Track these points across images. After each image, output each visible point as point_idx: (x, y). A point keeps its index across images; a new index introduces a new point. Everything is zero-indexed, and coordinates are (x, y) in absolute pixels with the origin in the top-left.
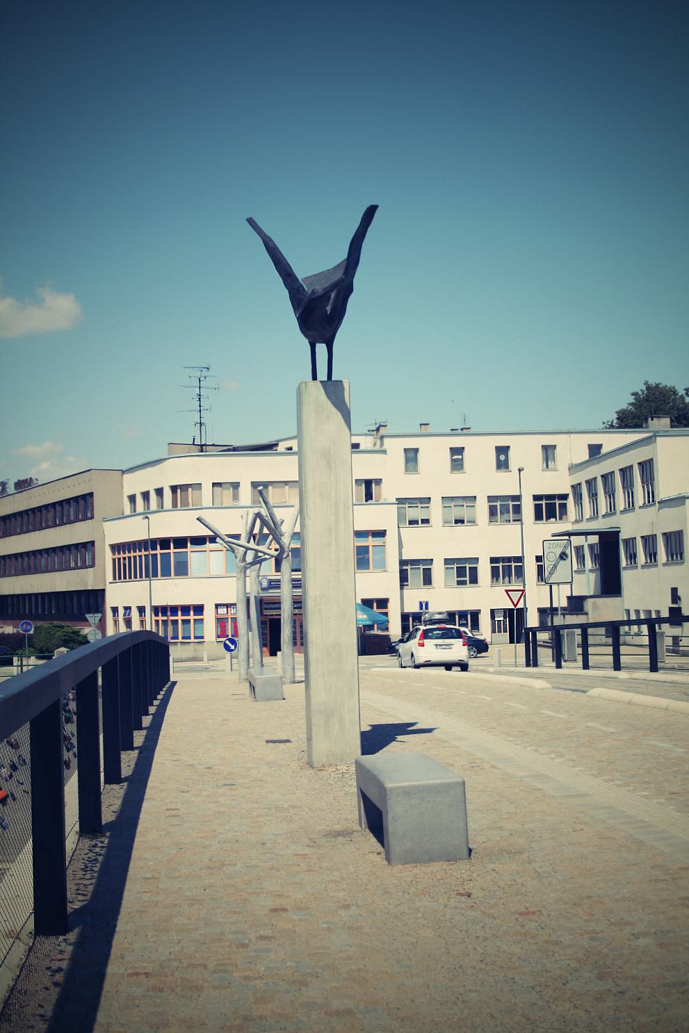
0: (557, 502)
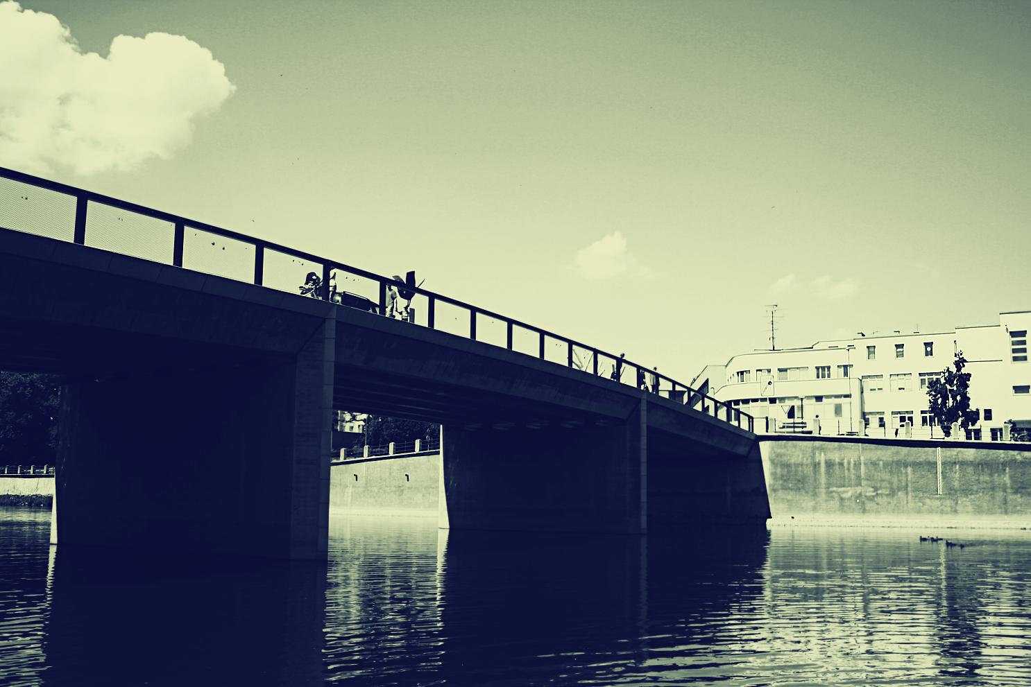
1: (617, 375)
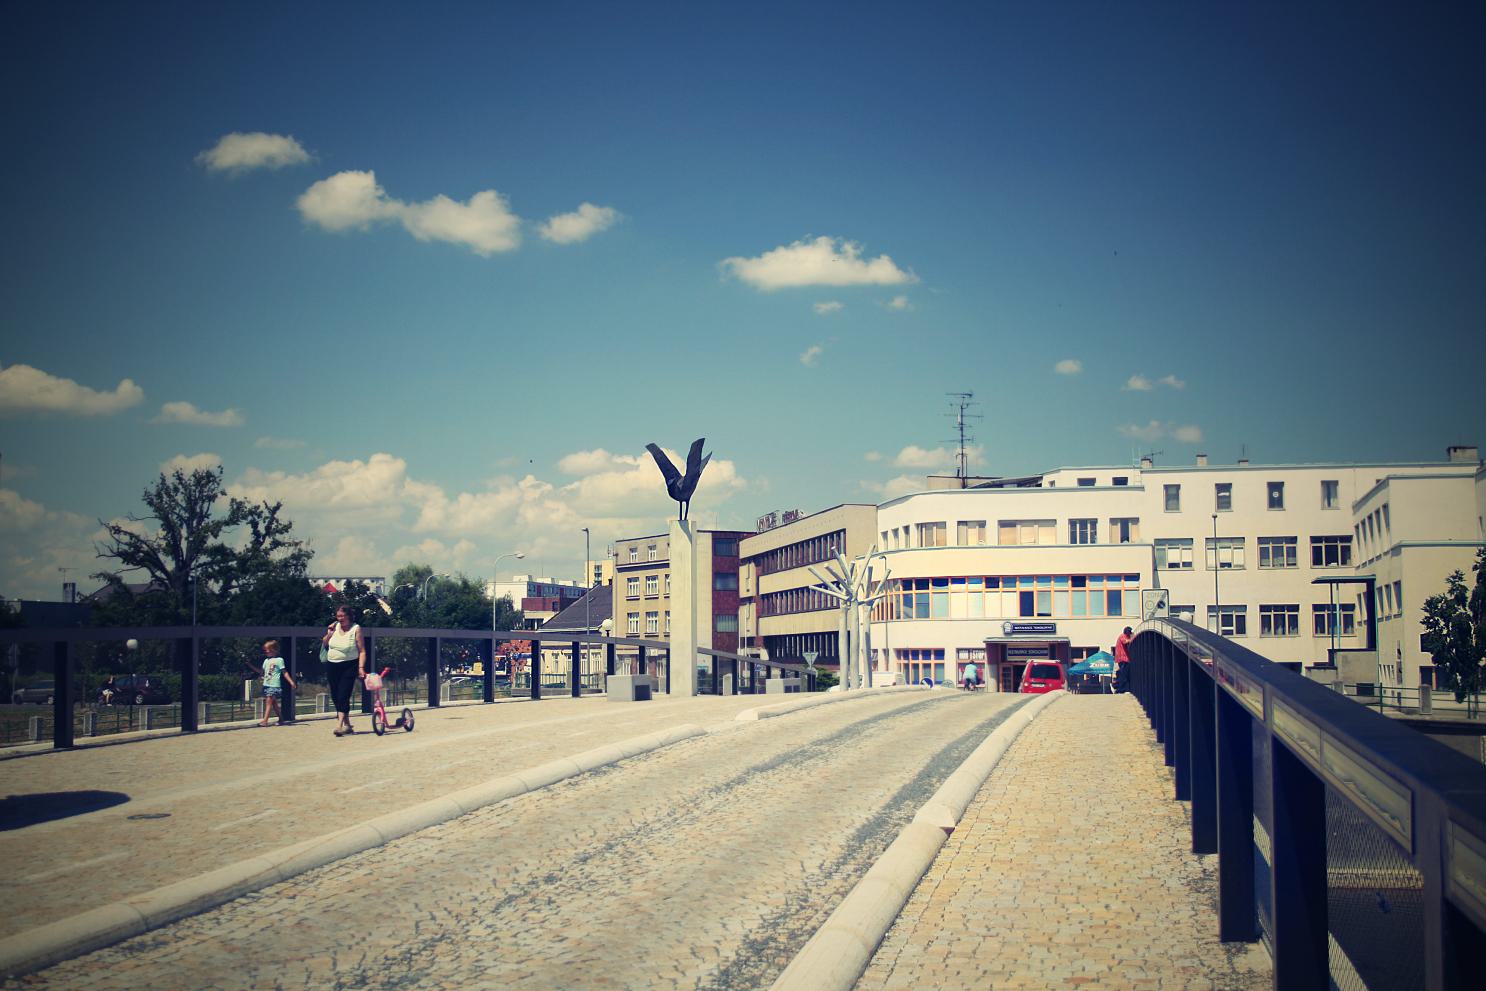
0: (1339, 545)
1: (1476, 698)
